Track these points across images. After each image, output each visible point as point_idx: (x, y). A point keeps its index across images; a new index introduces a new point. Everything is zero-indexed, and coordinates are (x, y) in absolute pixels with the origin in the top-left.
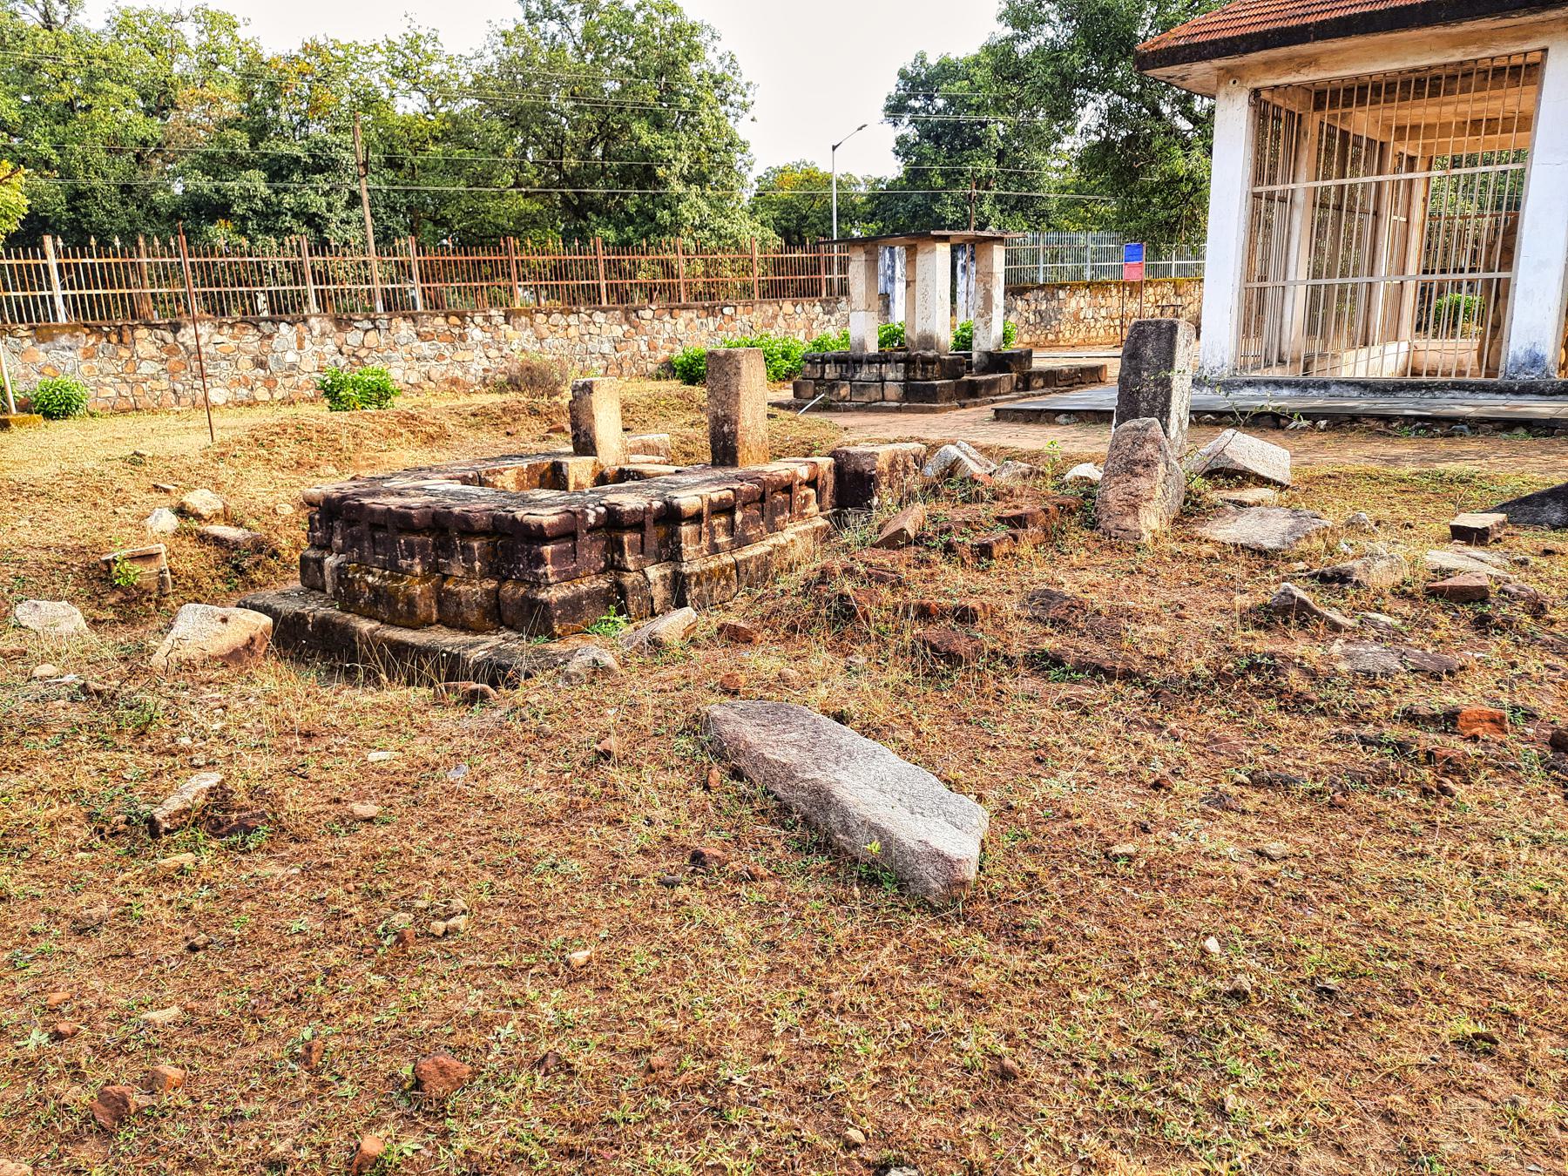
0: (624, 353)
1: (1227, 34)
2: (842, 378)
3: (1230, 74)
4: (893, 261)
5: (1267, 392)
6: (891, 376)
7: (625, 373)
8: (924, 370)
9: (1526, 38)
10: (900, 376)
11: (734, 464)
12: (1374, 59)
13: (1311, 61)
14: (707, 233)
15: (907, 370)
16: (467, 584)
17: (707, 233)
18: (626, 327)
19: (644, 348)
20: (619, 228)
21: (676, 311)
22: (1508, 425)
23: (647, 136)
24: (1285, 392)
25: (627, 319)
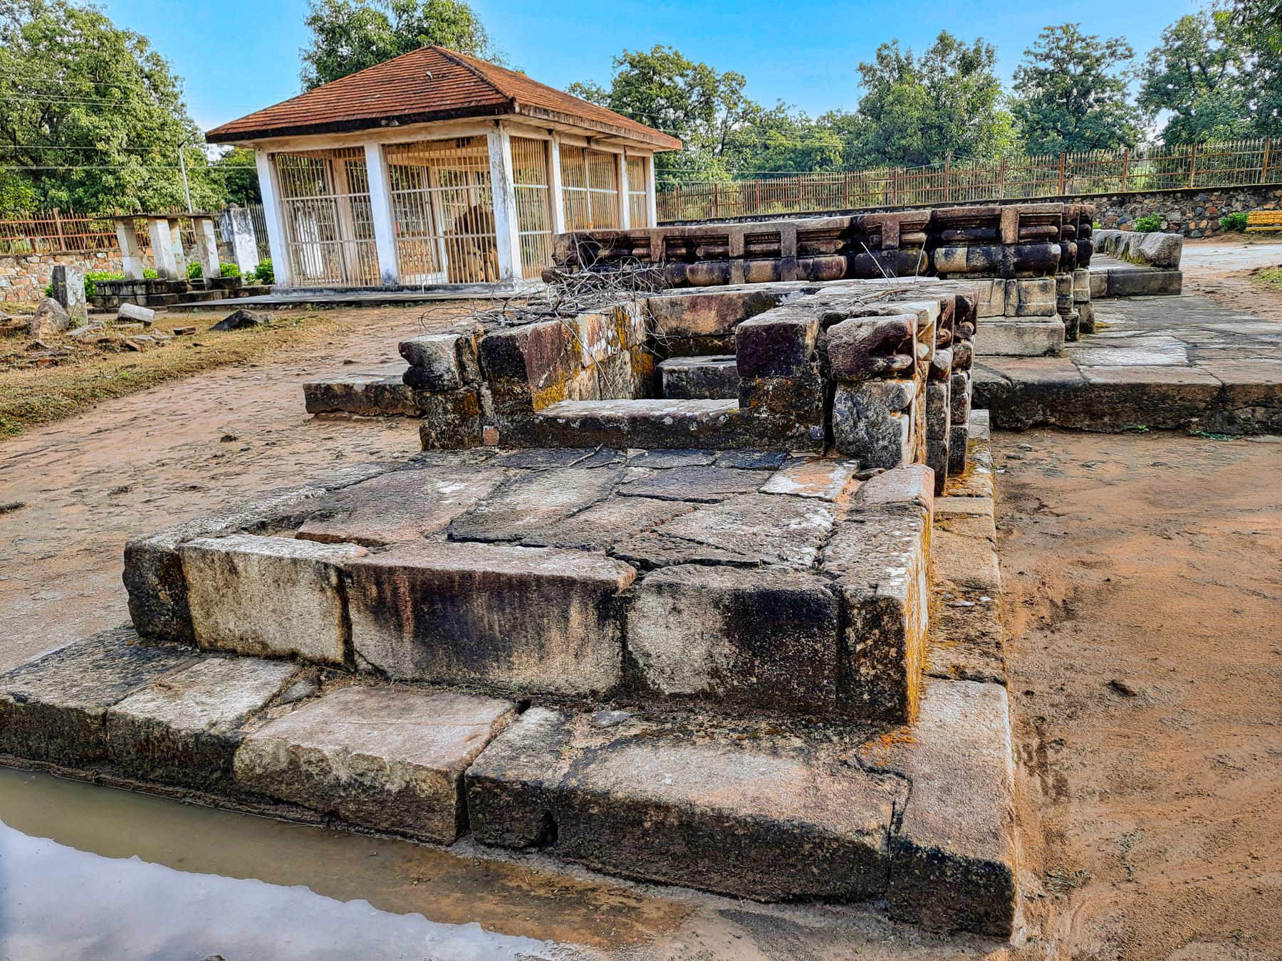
0: (19, 286)
1: (240, 130)
2: (113, 294)
3: (259, 147)
4: (230, 220)
5: (301, 294)
6: (139, 292)
7: (21, 299)
8: (156, 288)
9: (356, 141)
10: (144, 292)
11: (308, 388)
12: (309, 144)
13: (286, 143)
14: (151, 193)
15: (147, 289)
16: (626, 916)
17: (151, 193)
18: (18, 269)
19: (35, 282)
20: (71, 190)
21: (58, 257)
22: (349, 304)
23: (85, 120)
24: (308, 294)
25: (18, 263)
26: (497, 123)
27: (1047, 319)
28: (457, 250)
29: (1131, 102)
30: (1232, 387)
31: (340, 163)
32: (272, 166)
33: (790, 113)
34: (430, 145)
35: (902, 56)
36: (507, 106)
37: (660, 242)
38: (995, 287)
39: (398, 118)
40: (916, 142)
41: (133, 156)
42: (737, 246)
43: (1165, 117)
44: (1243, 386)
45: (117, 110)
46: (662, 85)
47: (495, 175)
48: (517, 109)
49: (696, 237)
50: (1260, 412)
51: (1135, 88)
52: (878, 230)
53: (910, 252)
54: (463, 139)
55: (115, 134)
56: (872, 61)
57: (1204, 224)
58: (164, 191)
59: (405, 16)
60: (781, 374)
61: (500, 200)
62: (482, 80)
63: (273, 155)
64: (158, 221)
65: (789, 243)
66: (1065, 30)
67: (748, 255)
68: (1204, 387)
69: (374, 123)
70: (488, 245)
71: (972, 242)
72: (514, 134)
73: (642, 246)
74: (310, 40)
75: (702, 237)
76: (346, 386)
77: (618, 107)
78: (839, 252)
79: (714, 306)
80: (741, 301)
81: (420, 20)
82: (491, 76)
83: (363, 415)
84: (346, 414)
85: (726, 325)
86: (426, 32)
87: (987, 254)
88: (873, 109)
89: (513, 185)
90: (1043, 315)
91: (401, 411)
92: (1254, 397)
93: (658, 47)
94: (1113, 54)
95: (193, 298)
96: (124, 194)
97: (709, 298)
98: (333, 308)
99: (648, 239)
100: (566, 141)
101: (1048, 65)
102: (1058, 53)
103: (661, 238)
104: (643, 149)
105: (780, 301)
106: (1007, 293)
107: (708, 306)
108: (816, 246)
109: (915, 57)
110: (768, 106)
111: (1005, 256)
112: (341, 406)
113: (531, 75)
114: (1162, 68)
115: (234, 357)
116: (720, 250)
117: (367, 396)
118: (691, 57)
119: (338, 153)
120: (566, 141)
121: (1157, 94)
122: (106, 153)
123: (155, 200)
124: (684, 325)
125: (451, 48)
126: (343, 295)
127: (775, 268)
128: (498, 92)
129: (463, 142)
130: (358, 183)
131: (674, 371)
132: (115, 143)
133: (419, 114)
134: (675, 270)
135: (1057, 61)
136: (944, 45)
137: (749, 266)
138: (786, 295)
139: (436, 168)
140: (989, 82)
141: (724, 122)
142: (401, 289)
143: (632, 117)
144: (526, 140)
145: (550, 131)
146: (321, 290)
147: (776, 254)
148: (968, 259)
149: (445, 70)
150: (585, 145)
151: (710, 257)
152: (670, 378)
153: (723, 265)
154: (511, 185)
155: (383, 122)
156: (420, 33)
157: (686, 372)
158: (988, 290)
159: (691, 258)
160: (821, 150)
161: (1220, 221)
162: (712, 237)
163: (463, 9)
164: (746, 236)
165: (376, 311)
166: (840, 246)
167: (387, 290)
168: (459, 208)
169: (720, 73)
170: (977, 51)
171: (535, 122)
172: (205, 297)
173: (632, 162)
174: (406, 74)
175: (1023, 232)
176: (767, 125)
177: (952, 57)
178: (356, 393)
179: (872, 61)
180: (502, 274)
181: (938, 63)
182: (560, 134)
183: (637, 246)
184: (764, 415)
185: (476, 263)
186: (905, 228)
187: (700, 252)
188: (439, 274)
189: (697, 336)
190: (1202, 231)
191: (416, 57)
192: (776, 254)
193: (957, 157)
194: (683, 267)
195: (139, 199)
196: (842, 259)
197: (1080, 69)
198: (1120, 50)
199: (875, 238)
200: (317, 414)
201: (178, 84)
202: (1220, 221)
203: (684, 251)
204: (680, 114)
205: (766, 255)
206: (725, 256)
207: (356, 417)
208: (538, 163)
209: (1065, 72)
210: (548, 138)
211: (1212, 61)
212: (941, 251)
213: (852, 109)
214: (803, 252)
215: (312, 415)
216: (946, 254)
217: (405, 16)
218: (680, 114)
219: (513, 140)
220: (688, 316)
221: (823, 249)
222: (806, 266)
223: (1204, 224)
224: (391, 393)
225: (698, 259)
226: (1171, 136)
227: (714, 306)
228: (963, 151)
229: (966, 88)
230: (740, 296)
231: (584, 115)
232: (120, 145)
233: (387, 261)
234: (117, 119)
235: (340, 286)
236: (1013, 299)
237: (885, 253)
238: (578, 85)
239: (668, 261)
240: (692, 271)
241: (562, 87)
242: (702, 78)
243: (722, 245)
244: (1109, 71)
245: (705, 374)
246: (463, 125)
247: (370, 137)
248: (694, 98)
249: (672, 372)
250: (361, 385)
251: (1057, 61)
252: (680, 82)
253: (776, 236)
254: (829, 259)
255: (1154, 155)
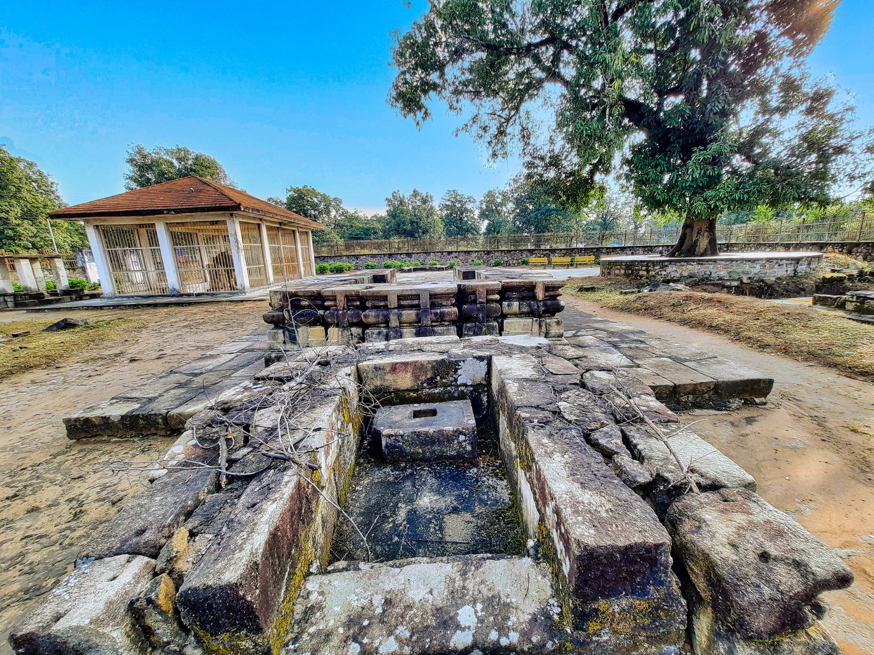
6: (9, 300)
11: (67, 422)
13: (105, 220)
14: (38, 239)
22: (149, 305)
26: (232, 215)
27: (560, 339)
28: (215, 276)
29: (476, 217)
30: (679, 386)
31: (143, 231)
32: (97, 232)
33: (360, 214)
34: (195, 224)
35: (401, 196)
36: (237, 207)
37: (343, 299)
38: (534, 323)
39: (174, 210)
40: (408, 227)
41: (26, 221)
42: (393, 302)
43: (486, 222)
44: (684, 385)
45: (14, 197)
46: (308, 201)
47: (232, 239)
48: (242, 209)
49: (367, 296)
50: (691, 397)
51: (477, 213)
52: (474, 293)
53: (492, 305)
54: (213, 222)
55: (12, 209)
56: (390, 197)
57: (514, 262)
58: (47, 238)
59: (183, 163)
60: (633, 593)
61: (236, 252)
62: (222, 194)
63: (97, 226)
64: (21, 260)
65: (425, 300)
66: (454, 191)
67: (400, 307)
68: (666, 386)
69: (160, 212)
70: (230, 273)
71: (521, 299)
72: (241, 220)
73: (331, 300)
74: (129, 170)
75: (370, 296)
76: (103, 418)
77: (290, 208)
78: (453, 305)
79: (410, 369)
80: (430, 365)
81: (191, 165)
82: (227, 192)
83: (121, 437)
84: (105, 438)
85: (419, 382)
86: (195, 171)
87: (529, 305)
88: (393, 215)
89: (242, 245)
90: (558, 337)
91: (155, 432)
92: (688, 390)
93: (305, 186)
94: (470, 201)
95: (49, 302)
96: (20, 240)
97: (406, 364)
98: (139, 308)
99: (335, 296)
100: (269, 224)
101: (449, 203)
102: (452, 199)
103: (344, 295)
104: (305, 228)
105: (459, 365)
106: (540, 326)
107: (405, 369)
108: (440, 302)
109: (406, 197)
110: (351, 211)
111: (538, 307)
112: (100, 432)
113: (249, 193)
114: (484, 207)
115: (44, 360)
116: (382, 304)
117: (123, 424)
118: (320, 190)
119: (141, 226)
120: (269, 224)
121: (483, 215)
122: (7, 219)
123: (41, 243)
124: (386, 384)
125: (208, 179)
126: (146, 300)
127: (417, 315)
128: (231, 200)
129: (216, 222)
130: (153, 240)
131: (392, 436)
132: (13, 214)
133: (186, 209)
134: (354, 314)
135: (452, 202)
136: (415, 194)
137: (401, 314)
138: (464, 361)
139: (201, 234)
140: (432, 208)
141: (335, 216)
142: (182, 295)
143: (296, 212)
144: (248, 223)
145: (261, 220)
146: (133, 297)
147: (417, 307)
148: (519, 308)
149: (201, 188)
150: (279, 226)
151: (375, 307)
152: (388, 440)
153: (385, 312)
154: (241, 245)
155: (165, 212)
156: (191, 171)
157: (402, 436)
158: (530, 324)
159: (363, 307)
160: (373, 228)
161: (520, 261)
162: (377, 296)
163: (214, 162)
164: (398, 296)
165: (165, 310)
166: (454, 302)
167: (173, 296)
168: (215, 252)
169: (332, 197)
170: (427, 196)
171: (252, 215)
172: (58, 301)
173: (301, 233)
174: (179, 189)
175: (547, 294)
176: (352, 218)
177: (419, 198)
178: (113, 422)
179: (390, 197)
180: (239, 287)
181: (414, 200)
182: (265, 220)
183: (327, 300)
184: (605, 638)
185: (224, 279)
186: (489, 292)
187: (369, 304)
188: (206, 283)
189: (397, 391)
190: (514, 264)
191: (186, 180)
192: (417, 307)
193: (424, 233)
194: (358, 313)
195: (31, 242)
196: (456, 309)
197: (459, 205)
198: (472, 200)
199: (473, 297)
200: (78, 440)
201: (54, 186)
202: (520, 261)
203: (358, 303)
204: (317, 213)
205: (410, 307)
206: (386, 307)
207: (114, 440)
208: (256, 233)
209: (455, 206)
210: (260, 222)
211: (498, 205)
212: (505, 303)
213: (383, 213)
214: (433, 305)
215: (74, 441)
216: (508, 305)
217: (183, 163)
218: (317, 213)
219: (241, 223)
220: (389, 377)
221: (444, 304)
222: (436, 314)
223: (514, 262)
224: (144, 420)
225: (368, 308)
226: (489, 230)
227: (410, 369)
228: (425, 232)
229: (425, 209)
230: (429, 362)
231: (278, 213)
232: (17, 214)
233: (172, 281)
234: (13, 202)
235: (144, 294)
236: (544, 329)
237: (479, 306)
238: (271, 198)
239: (348, 309)
240: (365, 316)
241: (264, 199)
242: (324, 198)
243: (383, 301)
244: (469, 206)
245: (418, 436)
246: (218, 215)
247: (158, 219)
248: (322, 206)
249: (390, 436)
250: (117, 416)
251: (452, 202)
252: (316, 200)
253: (417, 297)
254: (450, 310)
255: (484, 234)
